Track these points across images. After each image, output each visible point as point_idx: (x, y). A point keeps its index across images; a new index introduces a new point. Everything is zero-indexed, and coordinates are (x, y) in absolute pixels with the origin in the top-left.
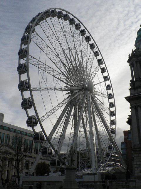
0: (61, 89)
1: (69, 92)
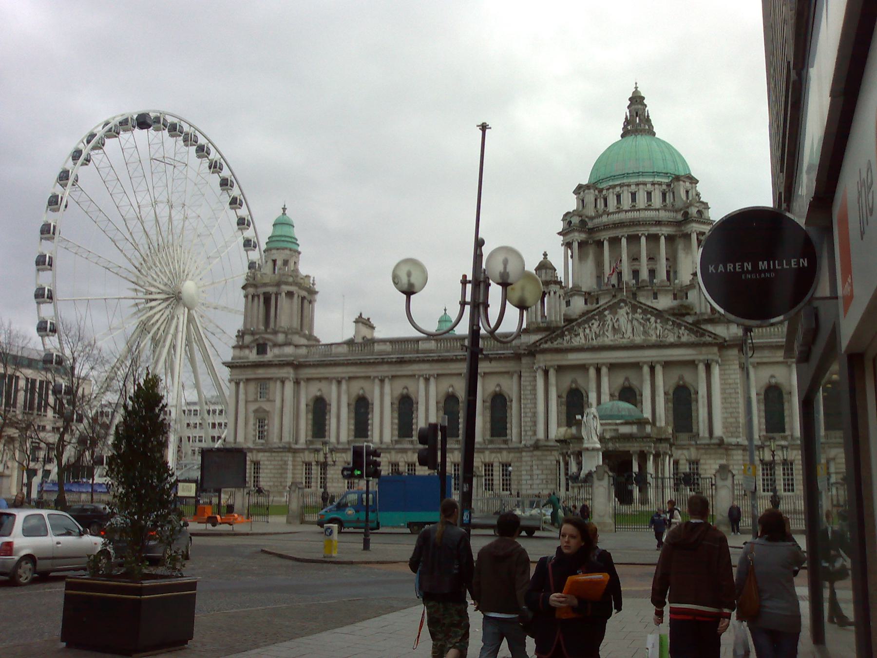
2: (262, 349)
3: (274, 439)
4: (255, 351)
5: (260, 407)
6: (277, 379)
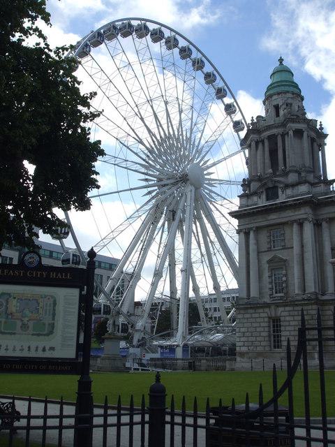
0: (221, 182)
1: (206, 177)
2: (272, 193)
3: (295, 289)
4: (264, 196)
5: (275, 257)
6: (293, 222)
